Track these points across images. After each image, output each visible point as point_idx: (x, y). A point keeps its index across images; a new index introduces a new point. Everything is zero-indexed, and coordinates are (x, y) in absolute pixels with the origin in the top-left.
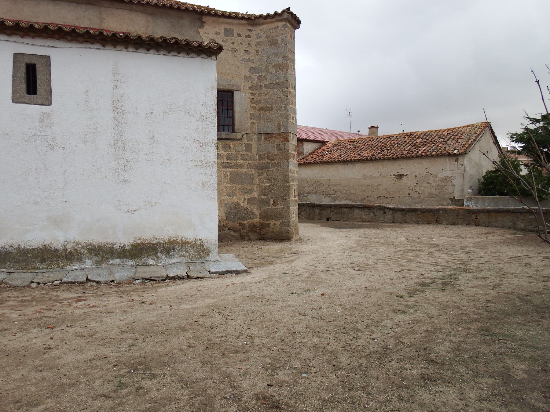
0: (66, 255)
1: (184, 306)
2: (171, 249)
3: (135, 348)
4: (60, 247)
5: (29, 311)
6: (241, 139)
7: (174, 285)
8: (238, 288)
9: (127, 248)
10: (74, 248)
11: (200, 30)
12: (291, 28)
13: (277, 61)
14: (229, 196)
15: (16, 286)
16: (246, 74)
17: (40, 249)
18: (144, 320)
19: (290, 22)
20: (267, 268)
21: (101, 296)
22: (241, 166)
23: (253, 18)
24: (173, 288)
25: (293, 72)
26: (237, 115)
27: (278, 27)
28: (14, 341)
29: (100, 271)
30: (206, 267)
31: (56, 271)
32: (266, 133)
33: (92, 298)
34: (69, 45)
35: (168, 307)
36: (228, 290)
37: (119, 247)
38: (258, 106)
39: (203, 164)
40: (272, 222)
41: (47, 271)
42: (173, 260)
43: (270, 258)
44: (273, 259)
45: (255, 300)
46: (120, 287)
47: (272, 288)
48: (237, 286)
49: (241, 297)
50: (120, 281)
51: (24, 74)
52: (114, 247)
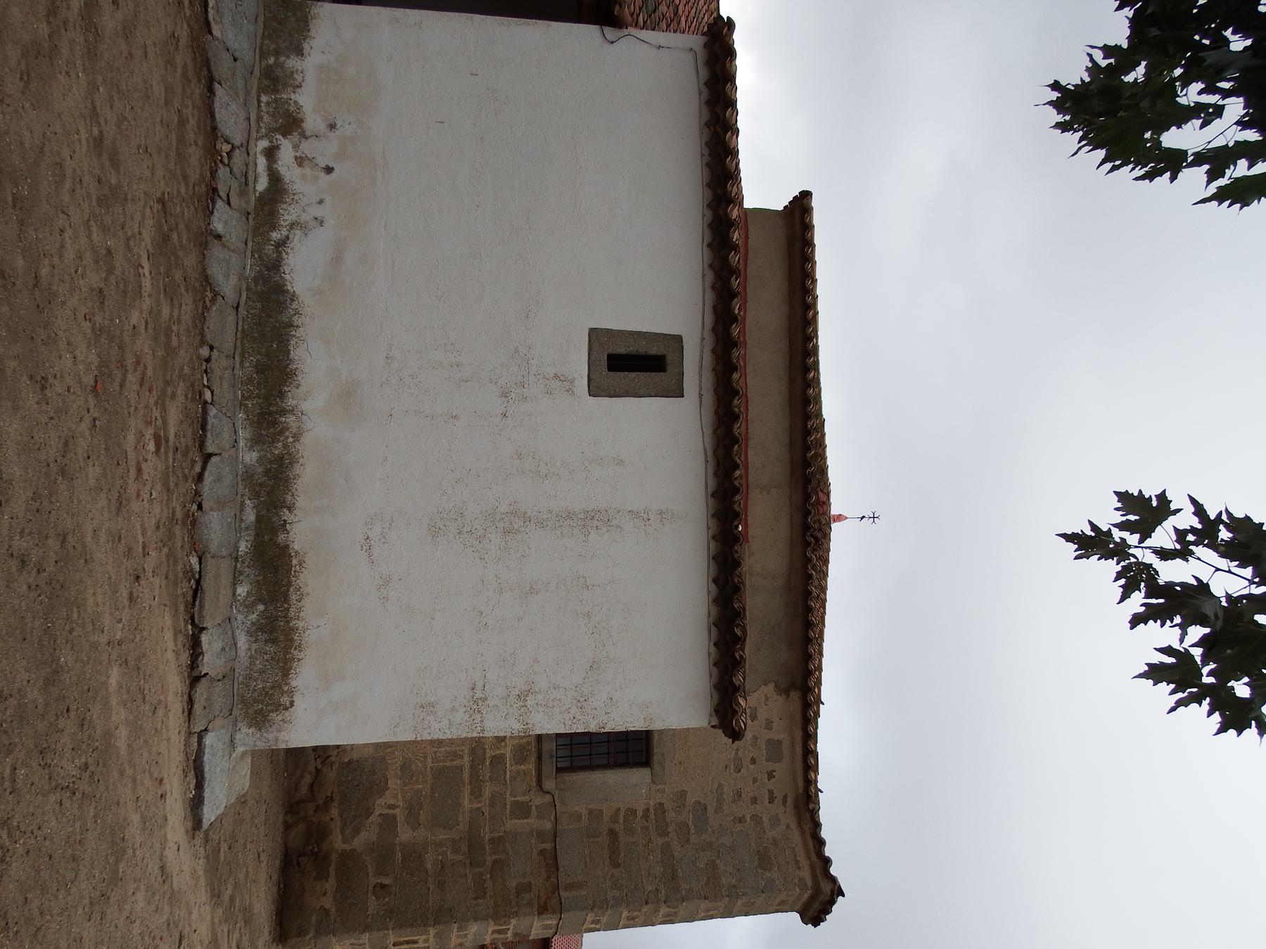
0: (271, 414)
1: (114, 676)
2: (272, 633)
3: (14, 569)
4: (291, 402)
5: (143, 344)
6: (541, 789)
7: (176, 645)
8: (153, 809)
9: (281, 537)
10: (287, 429)
11: (772, 686)
12: (801, 901)
13: (724, 871)
14: (403, 768)
15: (205, 319)
16: (689, 795)
17: (288, 365)
18: (89, 583)
19: (813, 898)
20: (203, 882)
21: (163, 484)
22: (476, 793)
23: (811, 806)
24: (171, 645)
25: (702, 915)
26: (596, 777)
27: (799, 868)
28: (72, 318)
29: (228, 479)
30: (218, 722)
31: (234, 393)
32: (558, 854)
33: (161, 467)
34: (708, 431)
35: (119, 635)
36: (148, 782)
37: (285, 521)
38: (619, 828)
39: (477, 703)
40: (331, 884)
41: (236, 377)
42: (242, 641)
43: (230, 888)
44: (226, 898)
45: (112, 859)
46: (184, 524)
47: (141, 904)
48: (157, 808)
49: (125, 820)
50: (200, 523)
51: (646, 352)
52: (285, 510)
